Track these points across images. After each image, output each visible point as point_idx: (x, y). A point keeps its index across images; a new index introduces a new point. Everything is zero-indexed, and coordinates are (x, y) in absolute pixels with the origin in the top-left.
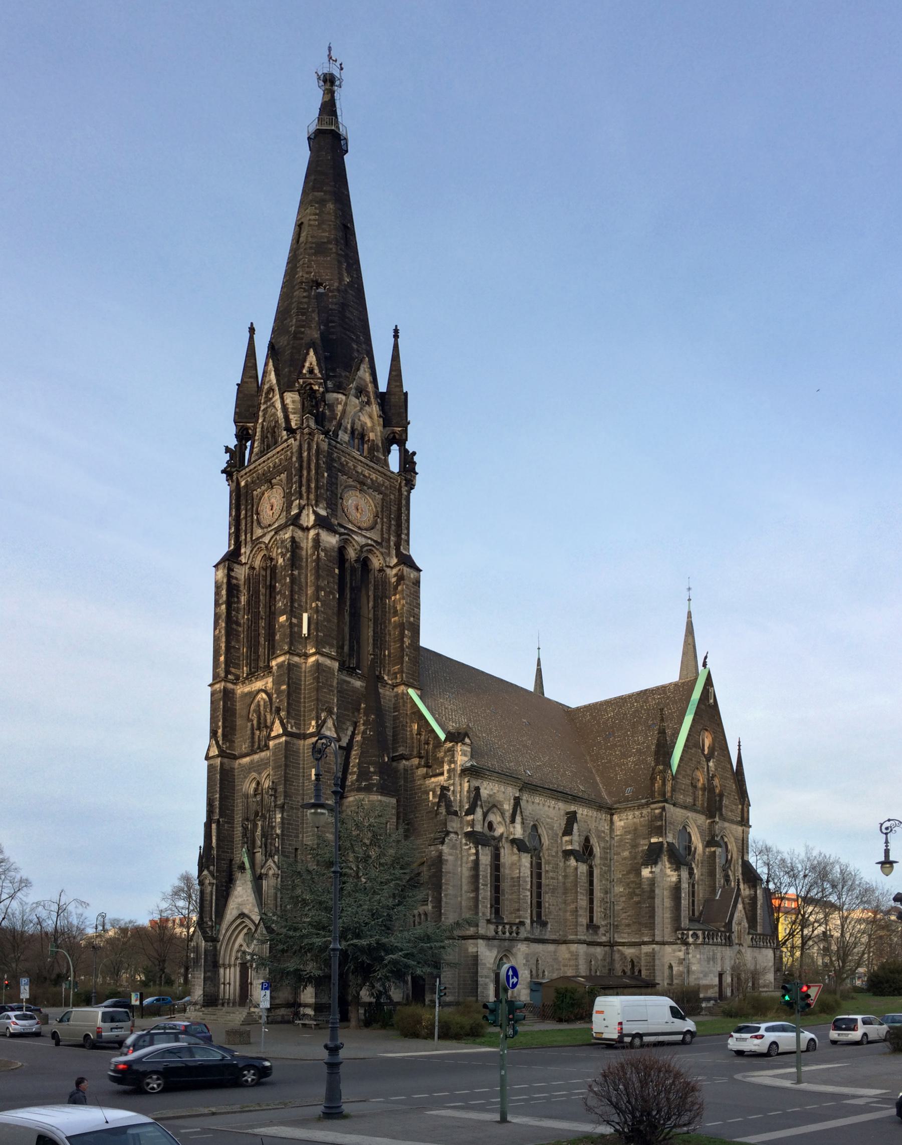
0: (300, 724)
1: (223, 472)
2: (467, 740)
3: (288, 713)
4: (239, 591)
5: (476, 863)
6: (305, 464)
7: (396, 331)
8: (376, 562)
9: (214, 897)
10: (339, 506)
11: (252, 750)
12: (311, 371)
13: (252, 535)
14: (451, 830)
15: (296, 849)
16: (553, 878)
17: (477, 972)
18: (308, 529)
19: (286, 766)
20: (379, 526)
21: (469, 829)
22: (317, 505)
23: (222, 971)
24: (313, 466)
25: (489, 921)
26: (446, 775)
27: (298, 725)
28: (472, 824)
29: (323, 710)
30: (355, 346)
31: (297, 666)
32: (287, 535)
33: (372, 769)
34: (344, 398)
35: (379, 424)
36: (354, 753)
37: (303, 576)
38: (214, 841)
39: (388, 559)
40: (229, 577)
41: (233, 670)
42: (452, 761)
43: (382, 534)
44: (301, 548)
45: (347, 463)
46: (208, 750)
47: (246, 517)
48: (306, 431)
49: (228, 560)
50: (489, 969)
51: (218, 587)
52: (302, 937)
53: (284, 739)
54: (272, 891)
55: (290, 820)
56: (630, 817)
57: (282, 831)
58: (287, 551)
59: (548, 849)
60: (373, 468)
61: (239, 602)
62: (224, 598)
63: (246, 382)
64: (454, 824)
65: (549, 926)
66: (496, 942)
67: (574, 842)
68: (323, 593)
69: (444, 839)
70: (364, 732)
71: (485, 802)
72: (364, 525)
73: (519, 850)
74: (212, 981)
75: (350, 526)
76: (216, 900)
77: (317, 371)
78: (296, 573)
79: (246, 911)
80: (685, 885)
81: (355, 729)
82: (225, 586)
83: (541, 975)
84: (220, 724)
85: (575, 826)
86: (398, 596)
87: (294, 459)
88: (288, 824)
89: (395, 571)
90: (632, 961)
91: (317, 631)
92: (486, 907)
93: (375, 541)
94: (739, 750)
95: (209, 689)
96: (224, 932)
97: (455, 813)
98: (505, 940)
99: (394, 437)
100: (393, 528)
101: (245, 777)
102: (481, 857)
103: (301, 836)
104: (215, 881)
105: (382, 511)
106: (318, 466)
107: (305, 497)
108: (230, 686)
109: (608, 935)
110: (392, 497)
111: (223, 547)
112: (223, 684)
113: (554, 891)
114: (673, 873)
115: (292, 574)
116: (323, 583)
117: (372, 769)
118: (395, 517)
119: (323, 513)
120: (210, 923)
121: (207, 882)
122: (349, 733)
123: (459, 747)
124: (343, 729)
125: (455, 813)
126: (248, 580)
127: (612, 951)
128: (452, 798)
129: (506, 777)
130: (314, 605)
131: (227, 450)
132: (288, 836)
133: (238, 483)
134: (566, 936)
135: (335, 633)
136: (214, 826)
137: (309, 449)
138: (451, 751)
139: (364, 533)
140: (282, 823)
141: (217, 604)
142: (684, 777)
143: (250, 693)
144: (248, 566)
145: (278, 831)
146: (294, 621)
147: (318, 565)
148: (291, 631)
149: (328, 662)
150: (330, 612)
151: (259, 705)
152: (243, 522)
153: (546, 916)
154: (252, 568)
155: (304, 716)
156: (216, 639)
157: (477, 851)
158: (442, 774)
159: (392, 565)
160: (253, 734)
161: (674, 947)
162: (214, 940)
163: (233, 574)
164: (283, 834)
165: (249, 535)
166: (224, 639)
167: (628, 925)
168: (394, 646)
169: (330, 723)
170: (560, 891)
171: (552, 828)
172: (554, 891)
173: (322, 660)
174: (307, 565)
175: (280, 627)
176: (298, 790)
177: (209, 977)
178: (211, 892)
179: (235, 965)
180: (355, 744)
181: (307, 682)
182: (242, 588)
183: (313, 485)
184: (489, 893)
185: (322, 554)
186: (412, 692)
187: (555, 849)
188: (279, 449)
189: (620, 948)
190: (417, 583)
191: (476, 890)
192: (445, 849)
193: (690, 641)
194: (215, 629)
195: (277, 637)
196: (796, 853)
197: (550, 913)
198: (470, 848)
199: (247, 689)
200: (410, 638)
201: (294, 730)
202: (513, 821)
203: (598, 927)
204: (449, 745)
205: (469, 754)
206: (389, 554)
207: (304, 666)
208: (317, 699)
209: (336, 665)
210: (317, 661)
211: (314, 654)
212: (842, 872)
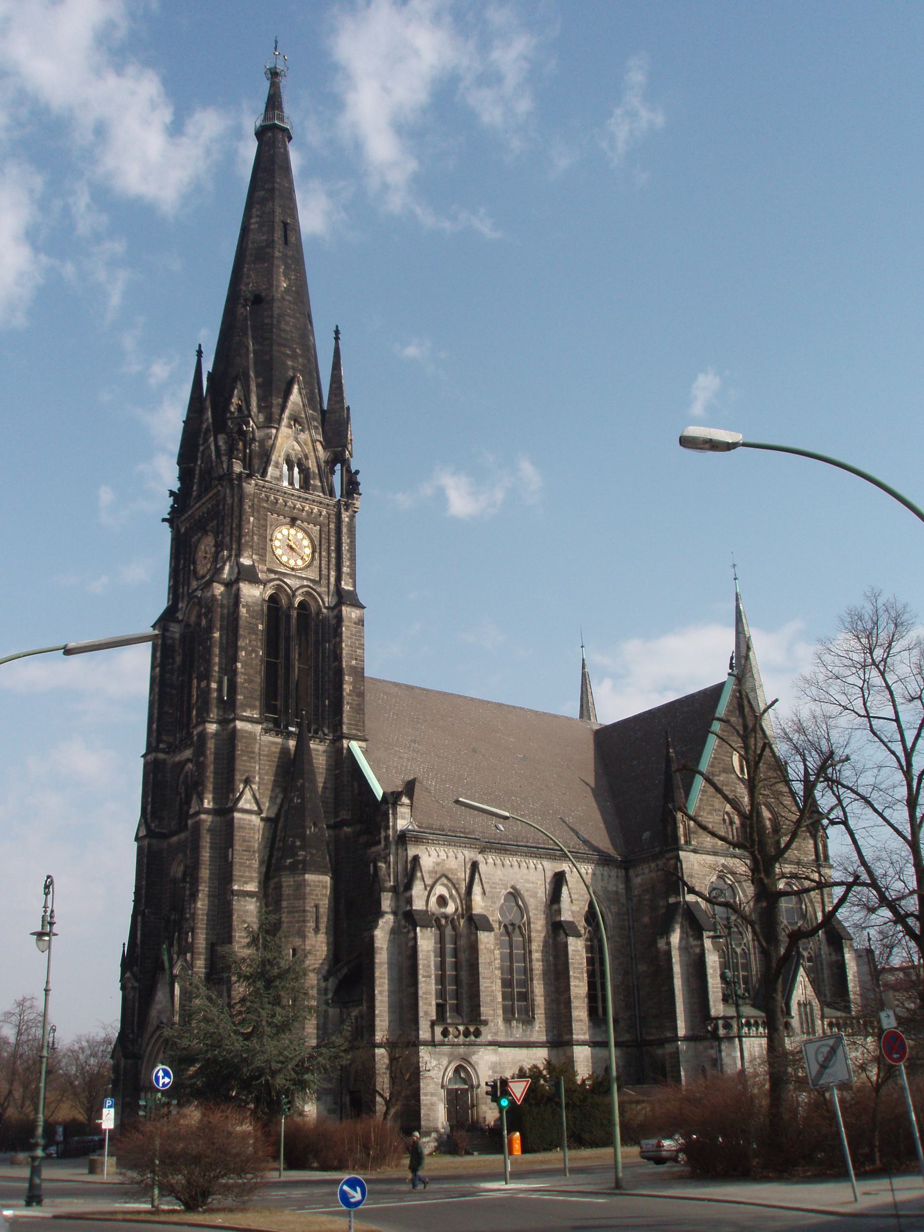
1: (164, 520)
7: (337, 332)
9: (137, 1005)
10: (269, 549)
30: (290, 363)
33: (298, 843)
41: (165, 738)
43: (320, 571)
46: (138, 830)
50: (437, 1084)
56: (647, 871)
61: (174, 663)
66: (446, 1049)
68: (243, 653)
85: (565, 890)
92: (430, 1004)
95: (142, 760)
104: (136, 985)
108: (161, 756)
112: (154, 754)
120: (131, 1036)
121: (130, 985)
126: (183, 637)
131: (172, 493)
136: (139, 918)
142: (710, 813)
143: (180, 762)
144: (184, 623)
154: (188, 625)
161: (706, 1043)
163: (168, 634)
165: (186, 588)
182: (177, 648)
184: (433, 987)
185: (243, 611)
188: (211, 495)
200: (351, 683)
212: (88, 1041)
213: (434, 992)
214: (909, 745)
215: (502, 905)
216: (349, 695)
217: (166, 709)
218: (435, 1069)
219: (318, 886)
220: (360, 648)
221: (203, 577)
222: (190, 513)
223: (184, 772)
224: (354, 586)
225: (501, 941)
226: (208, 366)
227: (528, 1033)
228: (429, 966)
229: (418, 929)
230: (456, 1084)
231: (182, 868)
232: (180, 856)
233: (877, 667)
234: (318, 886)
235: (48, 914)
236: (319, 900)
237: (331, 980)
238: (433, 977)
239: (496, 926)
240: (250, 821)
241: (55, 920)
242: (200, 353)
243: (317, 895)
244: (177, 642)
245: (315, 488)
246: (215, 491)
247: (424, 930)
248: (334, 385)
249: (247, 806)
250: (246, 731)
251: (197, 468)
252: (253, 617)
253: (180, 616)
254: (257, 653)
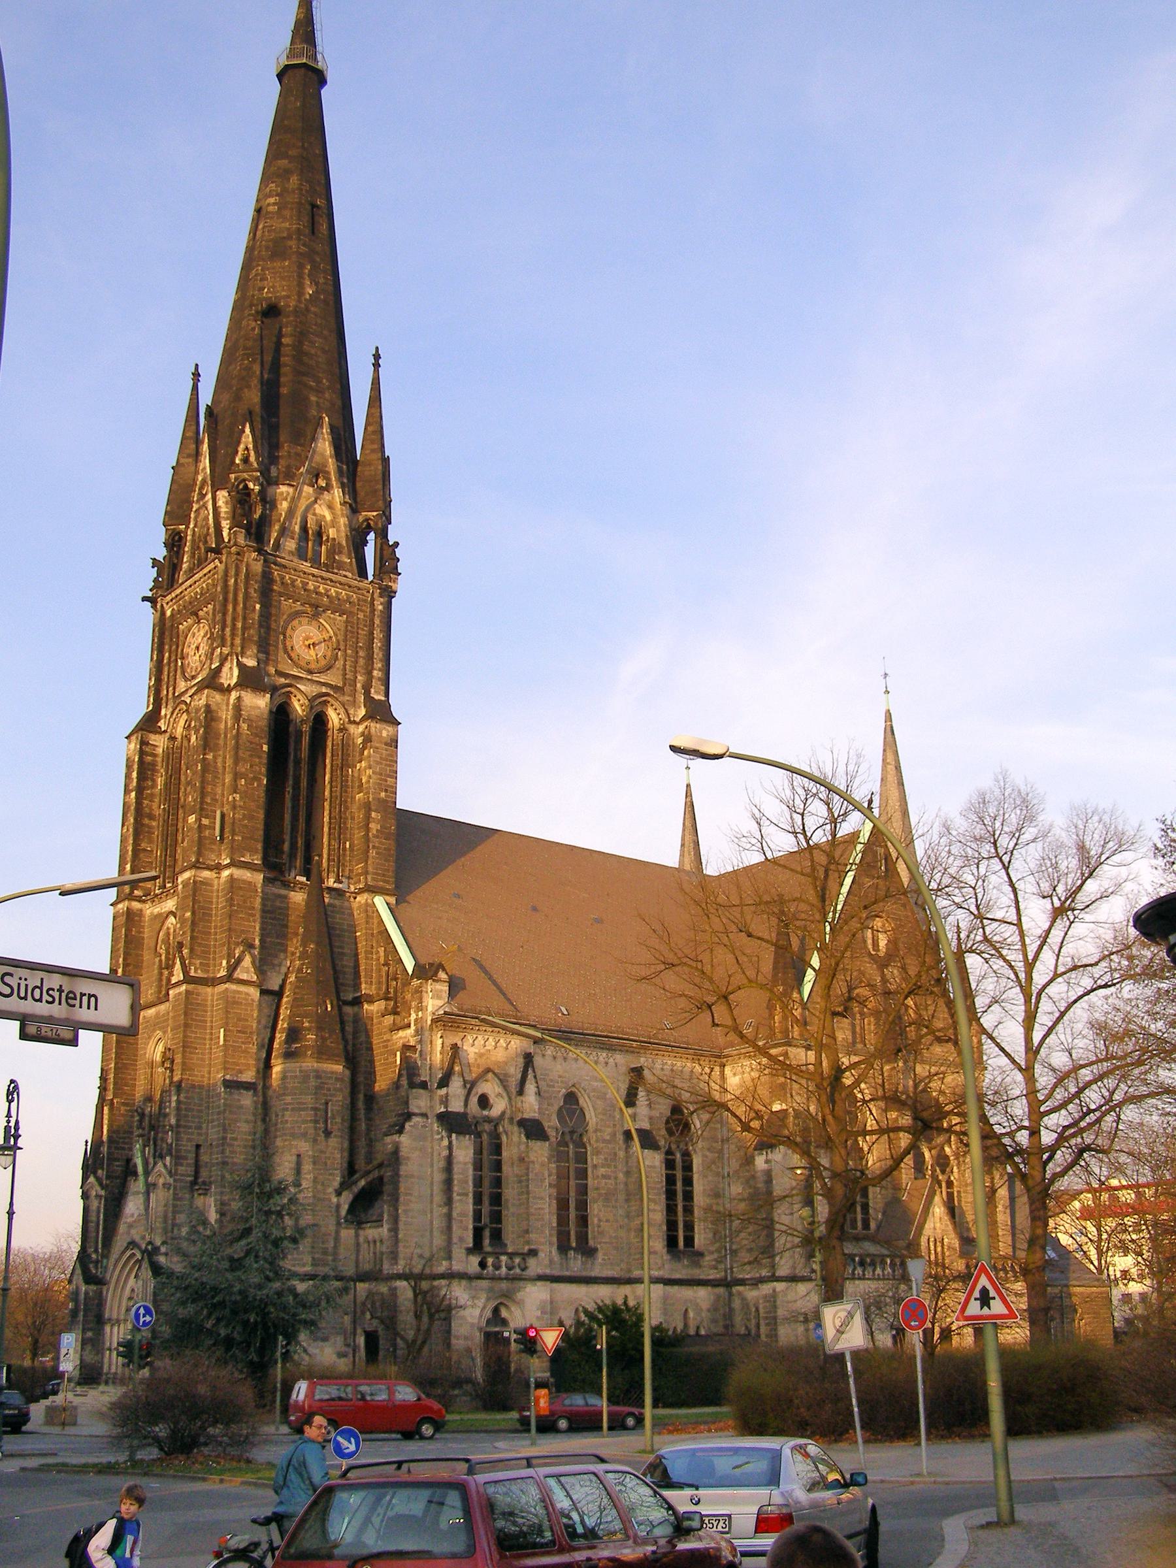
0: (208, 965)
1: (145, 599)
2: (442, 975)
3: (192, 950)
4: (154, 771)
5: (449, 1160)
6: (231, 596)
7: (377, 357)
8: (334, 717)
11: (159, 998)
12: (246, 460)
13: (174, 689)
14: (416, 1111)
15: (198, 1146)
16: (604, 1177)
17: (449, 1332)
18: (229, 690)
19: (186, 1025)
20: (339, 664)
21: (443, 1110)
22: (243, 654)
23: (108, 1328)
25: (470, 1251)
26: (413, 1027)
27: (205, 967)
28: (445, 1101)
29: (238, 944)
30: (313, 399)
31: (207, 883)
32: (201, 701)
33: (306, 1024)
34: (291, 490)
35: (343, 515)
36: (285, 1000)
37: (220, 760)
39: (351, 712)
40: (142, 753)
42: (420, 1008)
44: (218, 719)
45: (293, 581)
47: (169, 663)
48: (234, 549)
49: (142, 729)
50: (472, 1325)
53: (184, 987)
54: (161, 1209)
57: (178, 1120)
58: (201, 726)
59: (596, 1131)
60: (332, 581)
61: (154, 786)
62: (135, 784)
63: (183, 465)
64: (420, 1102)
65: (600, 1256)
66: (485, 1284)
67: (647, 1113)
70: (300, 970)
73: (528, 1137)
74: (93, 1345)
76: (105, 1220)
77: (252, 458)
78: (210, 757)
86: (363, 764)
87: (219, 589)
89: (361, 728)
91: (233, 833)
92: (466, 1229)
97: (424, 1085)
98: (500, 1279)
99: (369, 524)
100: (361, 662)
101: (150, 1038)
102: (456, 1152)
103: (204, 1126)
104: (103, 1193)
105: (345, 640)
106: (247, 596)
107: (229, 643)
108: (136, 905)
109: (722, 1266)
110: (361, 615)
111: (141, 708)
112: (126, 903)
113: (608, 1197)
115: (204, 759)
116: (242, 768)
118: (368, 643)
119: (251, 662)
123: (430, 986)
124: (274, 965)
125: (424, 1085)
126: (168, 754)
127: (731, 1294)
128: (419, 1063)
129: (511, 1020)
130: (231, 798)
132: (185, 1127)
133: (163, 613)
134: (629, 1271)
137: (237, 575)
138: (419, 991)
140: (178, 1109)
141: (127, 791)
143: (160, 915)
144: (168, 735)
145: (173, 1121)
146: (205, 822)
147: (237, 742)
148: (200, 837)
149: (247, 875)
150: (253, 805)
151: (168, 934)
152: (166, 669)
153: (594, 1238)
154: (173, 738)
155: (215, 952)
156: (123, 840)
158: (409, 1026)
160: (161, 974)
162: (100, 1282)
164: (178, 1126)
168: (358, 835)
169: (247, 961)
170: (622, 1197)
171: (603, 1096)
172: (608, 1197)
173: (238, 873)
174: (225, 744)
176: (203, 1060)
177: (90, 1340)
178: (99, 1208)
179: (126, 1320)
180: (288, 987)
181: (219, 904)
183: (239, 625)
185: (245, 726)
186: (380, 902)
187: (609, 1130)
188: (206, 571)
190: (394, 742)
191: (449, 1202)
192: (404, 1139)
193: (890, 759)
194: (123, 825)
197: (601, 1233)
199: (157, 910)
201: (200, 974)
202: (521, 1092)
203: (701, 1254)
204: (416, 982)
206: (354, 703)
207: (216, 882)
208: (230, 930)
209: (259, 878)
210: (231, 875)
211: (227, 866)
213: (471, 1213)
214: (1030, 957)
215: (561, 1108)
216: (374, 836)
217: (143, 845)
219: (330, 1078)
220: (391, 777)
221: (193, 677)
222: (178, 591)
223: (165, 928)
224: (387, 695)
225: (558, 1152)
226: (206, 398)
227: (589, 1266)
228: (467, 1182)
229: (454, 1135)
230: (496, 1326)
231: (161, 1048)
232: (159, 1033)
233: (1001, 859)
234: (330, 1078)
235: (12, 1124)
236: (331, 1095)
237: (345, 1194)
238: (471, 1195)
239: (552, 1133)
240: (247, 994)
241: (20, 1132)
242: (196, 375)
243: (329, 1090)
244: (159, 759)
245: (341, 566)
246: (212, 566)
247: (461, 1137)
248: (370, 429)
249: (244, 976)
250: (244, 881)
251: (189, 532)
252: (256, 735)
253: (162, 725)
254: (260, 780)
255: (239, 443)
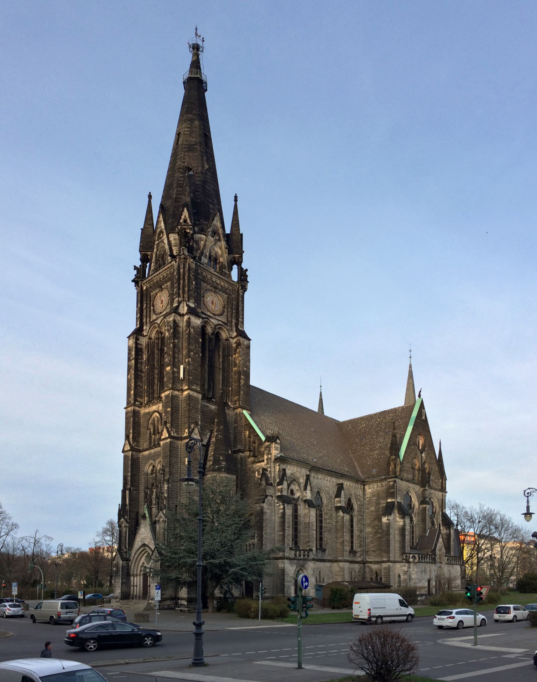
0: (179, 432)
1: (133, 281)
2: (278, 441)
3: (172, 424)
4: (142, 352)
5: (284, 514)
6: (181, 277)
8: (224, 335)
9: (127, 535)
10: (202, 301)
12: (185, 221)
13: (150, 318)
14: (268, 494)
15: (176, 506)
16: (329, 523)
18: (183, 315)
19: (170, 456)
20: (225, 314)
21: (279, 494)
22: (189, 301)
23: (132, 578)
24: (186, 278)
25: (291, 549)
26: (265, 461)
27: (177, 432)
28: (281, 491)
29: (192, 423)
31: (177, 396)
32: (171, 319)
33: (221, 458)
34: (205, 237)
35: (226, 253)
36: (211, 448)
37: (180, 343)
38: (127, 501)
39: (231, 333)
40: (136, 344)
41: (139, 399)
42: (269, 453)
43: (228, 318)
44: (179, 327)
45: (207, 276)
46: (124, 447)
47: (146, 308)
48: (182, 257)
49: (136, 333)
50: (291, 577)
51: (130, 350)
52: (180, 558)
53: (169, 440)
54: (162, 531)
55: (173, 488)
56: (375, 487)
57: (168, 495)
58: (171, 328)
59: (326, 506)
60: (222, 279)
61: (142, 358)
62: (134, 356)
63: (147, 228)
64: (270, 491)
65: (327, 551)
66: (295, 561)
68: (192, 353)
69: (264, 500)
70: (217, 436)
71: (289, 478)
72: (217, 313)
73: (309, 506)
74: (126, 584)
75: (208, 313)
76: (129, 536)
77: (188, 221)
78: (176, 341)
79: (147, 543)
80: (408, 527)
81: (211, 434)
82: (134, 349)
83: (322, 581)
84: (131, 431)
85: (343, 492)
86: (237, 355)
87: (175, 273)
88: (172, 491)
89: (235, 340)
90: (376, 573)
91: (189, 376)
92: (290, 540)
93: (223, 322)
94: (440, 446)
95: (125, 411)
96: (133, 555)
97: (271, 484)
98: (301, 560)
99: (235, 260)
100: (234, 314)
102: (286, 511)
103: (179, 498)
104: (128, 525)
105: (228, 305)
106: (189, 278)
107: (182, 296)
108: (137, 409)
109: (362, 557)
110: (234, 296)
111: (133, 326)
113: (330, 531)
114: (400, 520)
115: (174, 342)
116: (192, 347)
117: (221, 458)
118: (235, 308)
119: (192, 305)
120: (125, 550)
121: (123, 525)
122: (208, 437)
123: (273, 445)
124: (204, 434)
125: (271, 484)
126: (148, 345)
127: (365, 567)
128: (269, 476)
129: (301, 463)
130: (187, 360)
131: (135, 268)
132: (171, 498)
133: (142, 288)
134: (337, 557)
135: (200, 377)
136: (127, 492)
137: (184, 268)
138: (269, 447)
139: (216, 317)
140: (168, 490)
141: (129, 360)
142: (407, 463)
143: (149, 413)
144: (147, 337)
145: (166, 495)
146: (175, 370)
147: (189, 336)
148: (173, 376)
149: (195, 394)
150: (196, 364)
152: (145, 311)
153: (325, 545)
154: (150, 338)
155: (181, 426)
156: (129, 381)
157: (284, 507)
158: (263, 461)
159: (233, 336)
162: (127, 560)
163: (139, 342)
164: (168, 497)
165: (148, 319)
166: (133, 381)
167: (374, 551)
168: (235, 385)
169: (196, 431)
170: (334, 530)
171: (328, 493)
172: (330, 531)
173: (192, 393)
174: (183, 337)
175: (167, 374)
176: (177, 471)
177: (124, 582)
178: (126, 531)
179: (140, 575)
180: (211, 443)
181: (183, 406)
182: (144, 350)
183: (186, 289)
184: (291, 532)
185: (192, 330)
186: (245, 412)
187: (330, 506)
188: (166, 267)
189: (369, 564)
190: (248, 347)
191: (284, 530)
192: (265, 505)
193: (411, 382)
194: (128, 375)
195: (165, 380)
196: (474, 508)
197: (327, 544)
198: (280, 505)
199: (147, 410)
200: (244, 380)
201: (175, 435)
202: (305, 489)
203: (356, 552)
204: (267, 444)
205: (279, 449)
206: (232, 330)
207: (181, 396)
208: (189, 417)
209: (200, 396)
210: (189, 393)
211: (187, 390)
218: (511, 606)
251: (154, 256)
255: (181, 215)
